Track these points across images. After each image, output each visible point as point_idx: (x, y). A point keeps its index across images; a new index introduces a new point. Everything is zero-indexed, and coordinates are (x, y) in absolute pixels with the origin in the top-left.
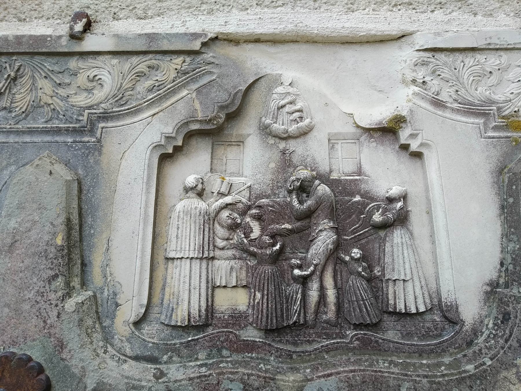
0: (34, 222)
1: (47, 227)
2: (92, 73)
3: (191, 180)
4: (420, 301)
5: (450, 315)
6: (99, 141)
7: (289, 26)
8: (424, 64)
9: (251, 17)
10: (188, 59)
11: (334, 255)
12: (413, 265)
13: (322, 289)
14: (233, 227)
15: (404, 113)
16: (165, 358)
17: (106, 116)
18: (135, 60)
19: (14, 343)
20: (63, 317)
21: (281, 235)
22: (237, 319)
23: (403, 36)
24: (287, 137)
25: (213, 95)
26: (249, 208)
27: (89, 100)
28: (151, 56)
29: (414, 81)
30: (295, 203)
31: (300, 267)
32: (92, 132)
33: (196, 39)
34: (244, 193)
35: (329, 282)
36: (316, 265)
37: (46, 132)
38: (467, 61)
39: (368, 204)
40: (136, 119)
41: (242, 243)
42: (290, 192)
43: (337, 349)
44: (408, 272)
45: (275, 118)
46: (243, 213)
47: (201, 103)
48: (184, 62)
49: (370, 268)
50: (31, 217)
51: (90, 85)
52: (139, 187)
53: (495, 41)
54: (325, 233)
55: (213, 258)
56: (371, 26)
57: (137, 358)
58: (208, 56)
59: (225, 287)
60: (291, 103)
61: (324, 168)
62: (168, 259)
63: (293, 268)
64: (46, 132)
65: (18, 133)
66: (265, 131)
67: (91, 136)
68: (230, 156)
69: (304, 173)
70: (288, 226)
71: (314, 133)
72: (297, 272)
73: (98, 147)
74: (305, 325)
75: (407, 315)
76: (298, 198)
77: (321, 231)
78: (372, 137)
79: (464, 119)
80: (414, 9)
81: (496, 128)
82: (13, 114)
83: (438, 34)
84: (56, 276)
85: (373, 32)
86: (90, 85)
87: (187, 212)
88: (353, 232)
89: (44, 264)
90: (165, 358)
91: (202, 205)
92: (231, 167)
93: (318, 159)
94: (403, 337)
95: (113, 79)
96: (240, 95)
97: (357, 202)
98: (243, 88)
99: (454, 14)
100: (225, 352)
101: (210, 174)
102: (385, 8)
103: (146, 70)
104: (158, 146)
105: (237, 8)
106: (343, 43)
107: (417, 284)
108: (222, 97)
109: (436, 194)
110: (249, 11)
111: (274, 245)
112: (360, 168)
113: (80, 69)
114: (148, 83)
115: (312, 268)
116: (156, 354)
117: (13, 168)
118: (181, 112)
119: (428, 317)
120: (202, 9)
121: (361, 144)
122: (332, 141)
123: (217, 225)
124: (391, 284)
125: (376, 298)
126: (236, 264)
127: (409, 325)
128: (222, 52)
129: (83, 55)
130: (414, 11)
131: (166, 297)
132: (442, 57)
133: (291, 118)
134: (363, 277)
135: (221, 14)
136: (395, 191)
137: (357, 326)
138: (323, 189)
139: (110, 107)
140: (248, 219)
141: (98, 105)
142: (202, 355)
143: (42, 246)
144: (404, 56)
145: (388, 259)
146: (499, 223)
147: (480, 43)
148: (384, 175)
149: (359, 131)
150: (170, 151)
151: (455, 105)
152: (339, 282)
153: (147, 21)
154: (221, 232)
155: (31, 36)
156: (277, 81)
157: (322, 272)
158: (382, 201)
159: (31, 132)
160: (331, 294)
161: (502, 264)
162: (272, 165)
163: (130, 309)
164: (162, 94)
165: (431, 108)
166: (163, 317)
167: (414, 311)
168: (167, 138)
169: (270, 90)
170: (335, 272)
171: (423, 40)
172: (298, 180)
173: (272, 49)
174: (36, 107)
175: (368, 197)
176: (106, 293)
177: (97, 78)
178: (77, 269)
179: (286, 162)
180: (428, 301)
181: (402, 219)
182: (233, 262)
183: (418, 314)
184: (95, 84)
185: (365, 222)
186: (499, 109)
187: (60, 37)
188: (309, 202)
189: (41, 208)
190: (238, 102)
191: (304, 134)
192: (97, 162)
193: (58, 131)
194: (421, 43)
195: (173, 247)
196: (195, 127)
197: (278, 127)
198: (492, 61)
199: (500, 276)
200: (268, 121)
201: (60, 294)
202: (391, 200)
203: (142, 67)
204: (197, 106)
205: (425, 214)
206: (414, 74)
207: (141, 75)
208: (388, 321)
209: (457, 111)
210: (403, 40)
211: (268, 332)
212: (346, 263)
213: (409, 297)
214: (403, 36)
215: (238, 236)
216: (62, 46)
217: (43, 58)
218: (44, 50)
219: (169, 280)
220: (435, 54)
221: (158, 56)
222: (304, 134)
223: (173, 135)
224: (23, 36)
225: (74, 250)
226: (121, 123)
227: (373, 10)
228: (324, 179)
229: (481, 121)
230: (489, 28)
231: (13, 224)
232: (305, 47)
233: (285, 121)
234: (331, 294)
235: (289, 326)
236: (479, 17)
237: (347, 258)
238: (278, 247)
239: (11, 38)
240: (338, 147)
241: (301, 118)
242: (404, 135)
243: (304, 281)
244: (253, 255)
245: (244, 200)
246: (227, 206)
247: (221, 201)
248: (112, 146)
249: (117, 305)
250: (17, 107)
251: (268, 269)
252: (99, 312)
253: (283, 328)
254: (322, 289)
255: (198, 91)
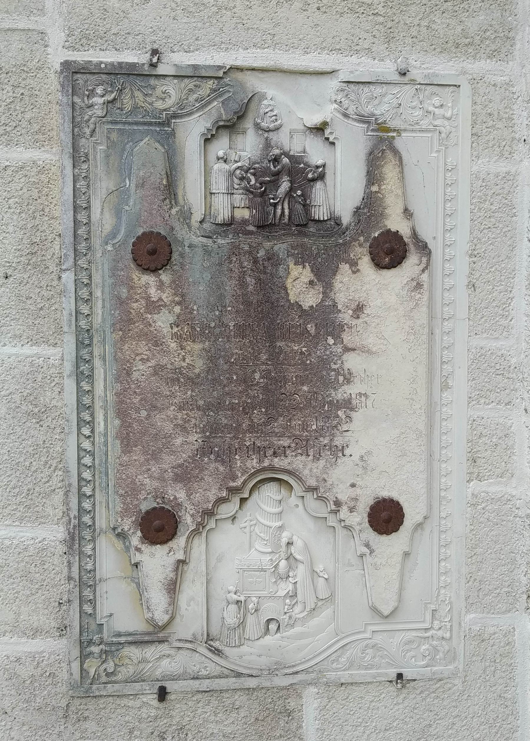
0: (152, 173)
1: (158, 176)
2: (164, 88)
3: (221, 153)
4: (325, 215)
5: (338, 222)
6: (173, 130)
7: (271, 62)
8: (342, 90)
9: (250, 55)
10: (216, 82)
11: (289, 194)
12: (324, 199)
13: (283, 209)
14: (242, 179)
15: (328, 120)
16: (215, 237)
17: (175, 116)
18: (186, 81)
19: (152, 227)
20: (171, 217)
21: (265, 183)
22: (245, 222)
23: (333, 72)
24: (269, 131)
25: (230, 105)
26: (249, 169)
27: (164, 105)
28: (195, 79)
29: (335, 101)
30: (272, 167)
31: (273, 199)
32: (169, 124)
33: (220, 69)
34: (246, 161)
35: (286, 206)
36: (280, 198)
37: (145, 124)
38: (365, 89)
39: (307, 169)
40: (191, 118)
41: (247, 186)
42: (269, 161)
43: (288, 234)
44: (321, 202)
45: (263, 119)
46: (247, 172)
47: (224, 110)
48: (214, 83)
49: (305, 200)
50: (149, 170)
51: (163, 95)
52: (196, 156)
53: (381, 78)
54: (285, 182)
55: (233, 194)
56: (316, 65)
57: (202, 236)
58: (227, 80)
59: (239, 207)
60: (271, 111)
61: (286, 149)
62: (211, 193)
63: (270, 199)
64: (145, 124)
65: (129, 124)
66: (257, 126)
67: (168, 127)
68: (239, 139)
69: (277, 152)
70: (268, 179)
71: (283, 128)
72: (272, 201)
73: (173, 134)
74: (275, 225)
75: (319, 221)
76: (273, 164)
77: (284, 181)
78: (312, 132)
79: (357, 125)
80: (342, 53)
81: (373, 130)
82: (124, 112)
83: (352, 72)
84: (165, 199)
85: (317, 69)
86: (163, 95)
87: (220, 170)
88: (299, 183)
89: (159, 193)
90: (215, 237)
91: (227, 167)
92: (240, 147)
93: (284, 144)
94: (317, 231)
95: (176, 93)
96: (245, 105)
97: (301, 167)
98: (246, 101)
99: (363, 58)
100: (240, 235)
101: (229, 150)
102: (325, 52)
103: (193, 87)
104: (204, 134)
105: (242, 48)
106: (301, 73)
107: (325, 207)
108: (236, 107)
109: (338, 165)
110: (249, 51)
111: (261, 188)
112: (305, 149)
113: (157, 85)
114: (195, 96)
115: (279, 199)
116: (211, 235)
117: (131, 144)
118: (214, 116)
119: (328, 222)
120: (222, 47)
121: (306, 136)
122: (291, 133)
123: (234, 177)
124: (313, 207)
125: (307, 214)
126: (244, 197)
127: (320, 226)
128: (234, 76)
129: (157, 76)
130: (342, 55)
131: (212, 211)
132: (352, 86)
133: (271, 120)
134: (301, 204)
135: (232, 52)
136: (320, 162)
137: (297, 226)
138: (285, 160)
139: (176, 110)
140: (249, 175)
141: (169, 108)
142: (231, 236)
143: (157, 185)
144: (332, 84)
145: (313, 196)
146: (365, 180)
147: (373, 80)
148: (316, 153)
149: (306, 128)
150: (210, 137)
151: (354, 117)
152: (291, 206)
153: (191, 54)
154: (236, 181)
155: (126, 63)
156: (263, 97)
157: (283, 201)
158: (314, 167)
159: (137, 123)
160: (287, 212)
161: (363, 199)
162: (261, 146)
163: (197, 216)
164: (204, 103)
165: (341, 117)
166: (212, 220)
167: (322, 219)
168: (208, 129)
169: (260, 101)
170: (289, 201)
171: (343, 76)
172: (273, 155)
173: (261, 75)
174: (136, 108)
175: (307, 165)
176: (186, 208)
177: (167, 91)
178: (173, 196)
179: (268, 145)
180: (329, 215)
181: (321, 177)
182: (242, 196)
183: (324, 221)
184: (166, 95)
185: (304, 177)
186: (376, 119)
187: (143, 64)
188: (279, 167)
189: (154, 166)
190: (243, 110)
191: (277, 129)
192: (174, 142)
193: (150, 124)
194: (342, 78)
195: (214, 187)
196: (221, 123)
197: (264, 125)
198: (378, 90)
199: (361, 205)
200: (259, 121)
201: (168, 207)
202: (317, 167)
203: (191, 86)
204: (223, 112)
205: (333, 174)
206: (336, 97)
207: (191, 90)
208: (311, 224)
209: (355, 120)
210: (333, 73)
211: (258, 227)
212: (294, 197)
213: (320, 213)
214: (333, 72)
215: (244, 183)
216: (145, 71)
217: (135, 77)
218: (136, 73)
219: (213, 203)
220: (349, 85)
221: (200, 79)
222: (277, 129)
223: (211, 128)
224: (122, 63)
225: (170, 189)
226: (184, 120)
227: (319, 53)
228: (286, 154)
229: (366, 126)
230: (379, 70)
231: (141, 173)
232: (279, 74)
233: (268, 121)
234: (287, 212)
235: (268, 225)
236: (376, 61)
237: (295, 195)
238: (263, 189)
239: (116, 64)
240: (294, 137)
241: (276, 120)
242: (327, 132)
243: (275, 205)
244: (252, 193)
245: (247, 165)
246: (238, 168)
247: (236, 165)
248: (180, 134)
249: (191, 213)
250: (125, 108)
251: (259, 199)
252: (186, 216)
253: (265, 226)
254: (283, 209)
255: (223, 103)
